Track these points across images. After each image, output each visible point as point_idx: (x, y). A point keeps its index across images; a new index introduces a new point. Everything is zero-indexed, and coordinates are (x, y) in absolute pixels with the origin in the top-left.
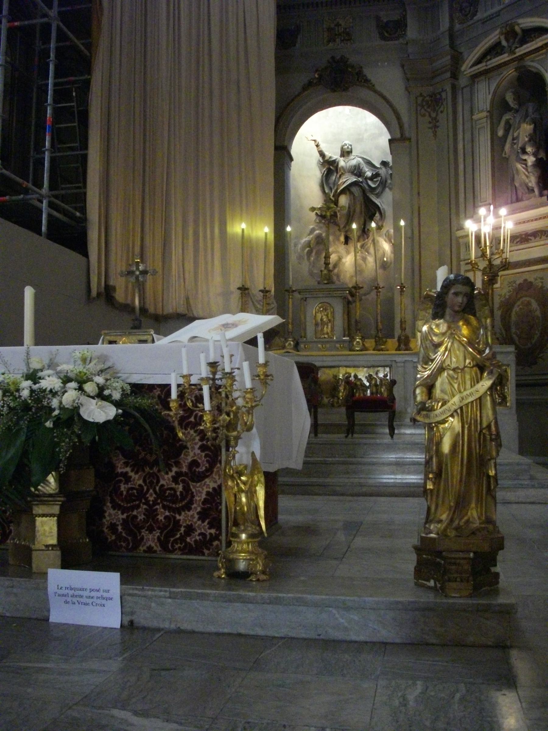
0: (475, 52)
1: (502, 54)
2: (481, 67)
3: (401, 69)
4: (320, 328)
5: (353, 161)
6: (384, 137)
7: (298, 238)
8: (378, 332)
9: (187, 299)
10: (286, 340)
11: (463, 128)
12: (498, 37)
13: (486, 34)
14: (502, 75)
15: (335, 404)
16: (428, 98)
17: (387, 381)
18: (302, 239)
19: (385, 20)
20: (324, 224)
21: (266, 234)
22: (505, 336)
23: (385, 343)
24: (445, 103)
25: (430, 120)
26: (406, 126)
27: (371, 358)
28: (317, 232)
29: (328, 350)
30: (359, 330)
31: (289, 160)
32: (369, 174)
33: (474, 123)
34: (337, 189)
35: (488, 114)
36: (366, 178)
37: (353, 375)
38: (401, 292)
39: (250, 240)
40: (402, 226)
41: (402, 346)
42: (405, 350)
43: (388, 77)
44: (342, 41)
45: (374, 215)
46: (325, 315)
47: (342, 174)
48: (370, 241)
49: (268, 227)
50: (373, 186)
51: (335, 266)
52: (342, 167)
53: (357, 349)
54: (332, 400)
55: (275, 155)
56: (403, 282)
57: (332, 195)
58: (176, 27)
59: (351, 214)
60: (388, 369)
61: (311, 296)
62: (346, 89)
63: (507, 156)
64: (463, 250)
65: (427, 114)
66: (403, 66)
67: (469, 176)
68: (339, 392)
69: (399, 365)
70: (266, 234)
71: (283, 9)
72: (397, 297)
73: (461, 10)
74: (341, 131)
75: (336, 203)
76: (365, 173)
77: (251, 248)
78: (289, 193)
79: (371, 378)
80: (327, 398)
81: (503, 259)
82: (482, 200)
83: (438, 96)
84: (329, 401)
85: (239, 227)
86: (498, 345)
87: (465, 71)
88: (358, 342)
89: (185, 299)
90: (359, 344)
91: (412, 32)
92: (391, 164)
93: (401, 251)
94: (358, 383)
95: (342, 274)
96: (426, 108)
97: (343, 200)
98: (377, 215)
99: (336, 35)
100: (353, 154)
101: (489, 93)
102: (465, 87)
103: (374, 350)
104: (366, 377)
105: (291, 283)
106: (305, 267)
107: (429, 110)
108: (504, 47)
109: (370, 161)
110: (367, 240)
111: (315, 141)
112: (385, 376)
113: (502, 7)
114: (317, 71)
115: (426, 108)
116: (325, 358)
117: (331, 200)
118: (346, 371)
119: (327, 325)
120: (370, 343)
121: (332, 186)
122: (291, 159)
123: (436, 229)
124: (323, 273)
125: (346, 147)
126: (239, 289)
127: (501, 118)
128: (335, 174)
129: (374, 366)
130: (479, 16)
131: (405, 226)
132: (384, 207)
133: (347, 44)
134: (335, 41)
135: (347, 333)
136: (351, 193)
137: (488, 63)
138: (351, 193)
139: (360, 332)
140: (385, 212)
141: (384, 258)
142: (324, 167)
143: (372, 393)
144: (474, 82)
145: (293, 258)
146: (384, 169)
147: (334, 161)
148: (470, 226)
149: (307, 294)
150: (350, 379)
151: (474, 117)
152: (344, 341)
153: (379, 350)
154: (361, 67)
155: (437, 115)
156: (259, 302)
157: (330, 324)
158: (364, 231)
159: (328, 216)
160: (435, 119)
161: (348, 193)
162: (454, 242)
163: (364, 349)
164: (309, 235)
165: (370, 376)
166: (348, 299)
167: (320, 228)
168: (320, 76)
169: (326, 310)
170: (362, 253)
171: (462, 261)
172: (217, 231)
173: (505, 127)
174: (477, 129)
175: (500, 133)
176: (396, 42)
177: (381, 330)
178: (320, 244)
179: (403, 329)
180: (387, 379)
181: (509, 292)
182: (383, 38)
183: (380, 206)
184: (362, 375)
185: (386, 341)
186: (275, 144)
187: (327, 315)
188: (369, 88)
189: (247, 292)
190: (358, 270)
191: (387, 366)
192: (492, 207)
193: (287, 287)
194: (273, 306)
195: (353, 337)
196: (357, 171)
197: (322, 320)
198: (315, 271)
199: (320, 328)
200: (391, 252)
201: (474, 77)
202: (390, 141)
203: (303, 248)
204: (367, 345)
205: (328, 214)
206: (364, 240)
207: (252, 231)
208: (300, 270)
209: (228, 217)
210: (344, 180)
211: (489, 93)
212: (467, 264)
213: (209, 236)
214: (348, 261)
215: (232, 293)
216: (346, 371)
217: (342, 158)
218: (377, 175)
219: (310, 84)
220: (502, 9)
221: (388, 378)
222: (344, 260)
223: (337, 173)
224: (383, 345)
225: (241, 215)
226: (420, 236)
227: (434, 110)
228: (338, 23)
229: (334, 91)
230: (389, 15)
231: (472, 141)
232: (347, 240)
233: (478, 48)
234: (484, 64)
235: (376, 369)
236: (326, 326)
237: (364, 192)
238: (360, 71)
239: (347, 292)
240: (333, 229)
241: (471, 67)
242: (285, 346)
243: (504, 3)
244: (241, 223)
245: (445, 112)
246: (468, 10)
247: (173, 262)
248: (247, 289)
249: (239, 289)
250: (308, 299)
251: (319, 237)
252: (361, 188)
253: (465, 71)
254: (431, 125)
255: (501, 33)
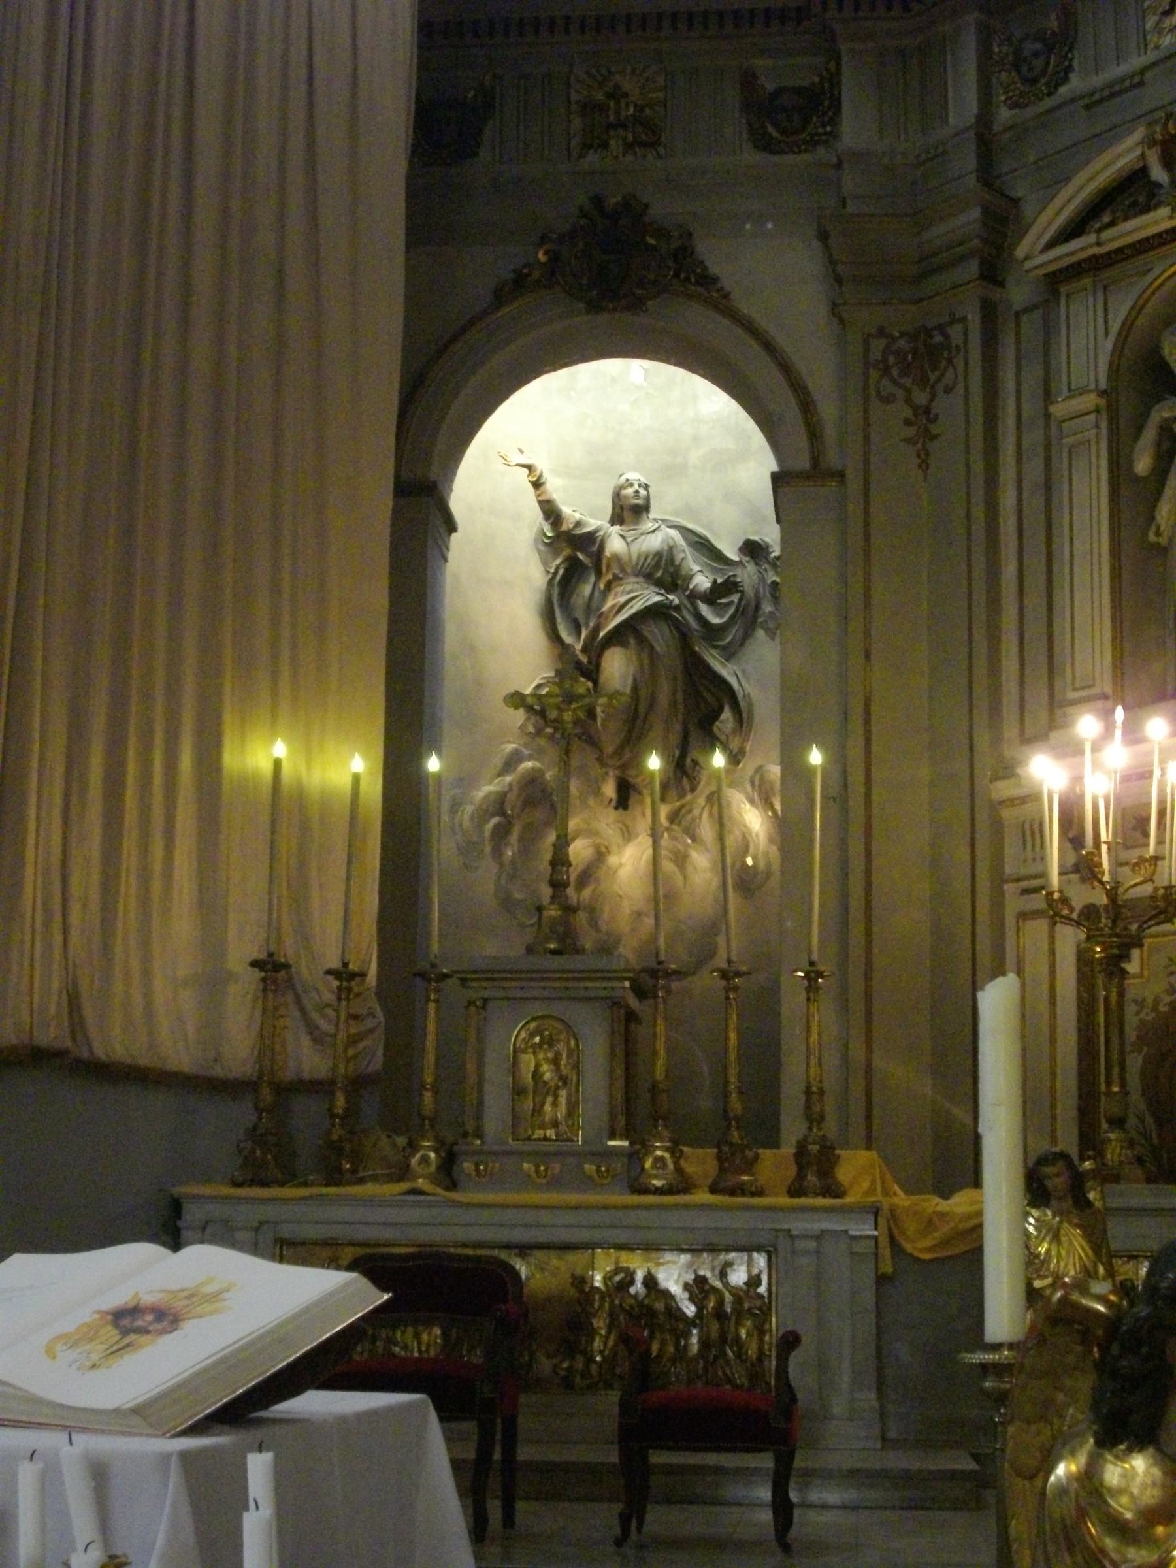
0: (1058, 202)
1: (1147, 209)
2: (1082, 247)
3: (816, 244)
4: (529, 1104)
5: (653, 538)
6: (756, 464)
7: (465, 781)
8: (729, 1127)
9: (74, 1003)
10: (413, 1146)
11: (1019, 446)
12: (1138, 152)
13: (1104, 139)
14: (1148, 278)
15: (578, 1379)
16: (902, 343)
17: (758, 1303)
18: (478, 790)
19: (770, 87)
20: (551, 737)
21: (356, 778)
22: (1155, 1141)
23: (750, 1165)
24: (959, 362)
25: (907, 412)
26: (830, 433)
27: (703, 1221)
28: (529, 764)
29: (555, 1183)
30: (665, 1118)
31: (442, 530)
32: (702, 582)
33: (1053, 428)
34: (597, 629)
35: (1103, 402)
36: (694, 596)
37: (640, 1276)
38: (808, 990)
39: (301, 797)
40: (815, 767)
41: (811, 1178)
42: (816, 1195)
43: (776, 272)
44: (629, 147)
45: (716, 714)
46: (547, 1060)
47: (616, 578)
48: (702, 801)
49: (365, 757)
50: (715, 620)
51: (586, 877)
52: (616, 557)
53: (657, 1183)
54: (565, 1365)
55: (397, 514)
56: (815, 957)
57: (578, 647)
58: (78, 79)
59: (642, 710)
60: (761, 1260)
61: (501, 994)
62: (636, 305)
63: (1163, 541)
64: (1011, 849)
65: (900, 394)
66: (824, 237)
67: (1035, 601)
68: (592, 1333)
69: (801, 1245)
70: (356, 778)
71: (438, 35)
72: (792, 1000)
73: (1016, 66)
74: (612, 441)
75: (591, 672)
76: (691, 577)
77: (305, 828)
78: (438, 638)
79: (702, 1291)
80: (549, 1356)
81: (1156, 889)
82: (1077, 685)
83: (938, 339)
84: (555, 1366)
85: (264, 753)
86: (1145, 1185)
87: (1027, 258)
88: (661, 1159)
89: (65, 997)
90: (665, 1165)
91: (857, 125)
92: (776, 552)
93: (811, 849)
94: (659, 1306)
95: (607, 909)
96: (895, 372)
97: (617, 667)
98: (727, 714)
99: (610, 126)
100: (652, 515)
101: (1107, 334)
102: (1026, 310)
103: (713, 1190)
104: (686, 1287)
105: (435, 947)
106: (485, 878)
107: (907, 381)
108: (1159, 185)
109: (707, 540)
110: (689, 797)
111: (529, 467)
112: (754, 1281)
113: (1151, 56)
114: (543, 240)
115: (895, 372)
116: (545, 1217)
117: (576, 668)
118: (617, 1262)
119: (556, 1096)
120: (700, 1162)
121: (579, 615)
122: (451, 526)
123: (925, 772)
124: (545, 913)
125: (630, 491)
126: (255, 964)
127: (1144, 416)
128: (592, 579)
129: (713, 1249)
130: (1076, 83)
131: (824, 767)
132: (749, 689)
133: (644, 157)
134: (605, 146)
135: (622, 1121)
136: (642, 640)
137: (1107, 234)
138: (642, 640)
139: (666, 1127)
140: (750, 705)
141: (745, 857)
142: (556, 553)
143: (705, 1344)
144: (1056, 294)
145: (444, 849)
146: (751, 568)
147: (591, 537)
148: (1045, 772)
149: (488, 985)
150: (632, 1290)
151: (1052, 409)
152: (615, 1151)
153: (732, 1193)
154: (690, 234)
155: (933, 396)
156: (322, 1007)
157: (563, 1093)
158: (683, 770)
159: (567, 715)
160: (927, 410)
161: (632, 641)
162: (982, 817)
163: (682, 1185)
164: (499, 775)
165: (701, 1281)
166: (627, 1006)
167: (538, 754)
168: (554, 257)
169: (550, 1042)
170: (674, 838)
171: (1007, 882)
172: (186, 762)
173: (1159, 445)
174: (1066, 450)
175: (1143, 464)
176: (807, 157)
177: (738, 1119)
178: (535, 806)
179: (814, 1118)
180: (761, 1296)
181: (1167, 992)
182: (764, 144)
183: (735, 685)
184: (673, 1275)
185: (757, 1156)
186: (397, 476)
187: (556, 1061)
188: (709, 303)
189: (282, 974)
190: (661, 892)
191: (758, 1249)
192: (1120, 713)
193: (423, 965)
194: (369, 1023)
195: (643, 1143)
196: (663, 571)
197: (537, 1074)
198: (518, 895)
199: (529, 1104)
200: (771, 840)
201: (1057, 281)
202: (776, 478)
203: (482, 815)
204: (690, 1168)
205: (568, 716)
206: (681, 796)
207: (309, 768)
208: (465, 878)
209: (228, 718)
210: (622, 599)
211: (1107, 334)
212: (1025, 892)
213: (158, 779)
214: (629, 862)
215: (230, 977)
216: (617, 1262)
217: (617, 528)
218: (730, 586)
219: (519, 283)
220: (1154, 64)
221: (762, 1289)
222: (613, 860)
223: (599, 574)
224: (743, 1173)
225: (274, 716)
226: (868, 795)
227: (923, 381)
228: (617, 86)
229: (594, 307)
230: (783, 69)
231: (1048, 487)
232: (625, 795)
233: (1070, 189)
234: (1092, 238)
235: (723, 1257)
236: (550, 1099)
237: (683, 636)
238: (684, 248)
239: (627, 984)
240: (582, 756)
241: (1050, 245)
242: (409, 1165)
243: (1157, 47)
244: (272, 741)
245: (960, 389)
246: (1039, 63)
247: (29, 870)
248: (286, 966)
249: (255, 964)
250: (490, 1004)
251: (532, 781)
252: (677, 628)
253: (1027, 258)
254: (911, 432)
255: (1150, 142)
